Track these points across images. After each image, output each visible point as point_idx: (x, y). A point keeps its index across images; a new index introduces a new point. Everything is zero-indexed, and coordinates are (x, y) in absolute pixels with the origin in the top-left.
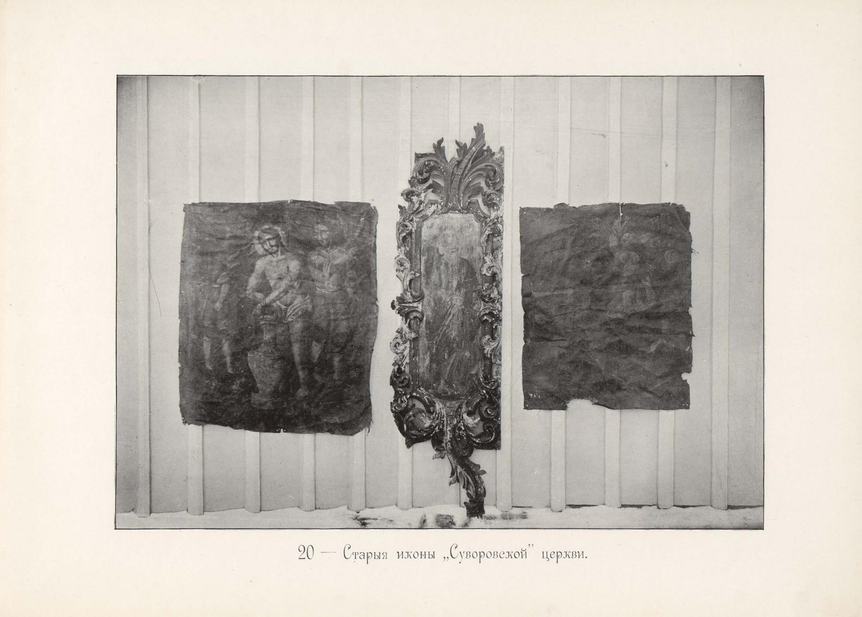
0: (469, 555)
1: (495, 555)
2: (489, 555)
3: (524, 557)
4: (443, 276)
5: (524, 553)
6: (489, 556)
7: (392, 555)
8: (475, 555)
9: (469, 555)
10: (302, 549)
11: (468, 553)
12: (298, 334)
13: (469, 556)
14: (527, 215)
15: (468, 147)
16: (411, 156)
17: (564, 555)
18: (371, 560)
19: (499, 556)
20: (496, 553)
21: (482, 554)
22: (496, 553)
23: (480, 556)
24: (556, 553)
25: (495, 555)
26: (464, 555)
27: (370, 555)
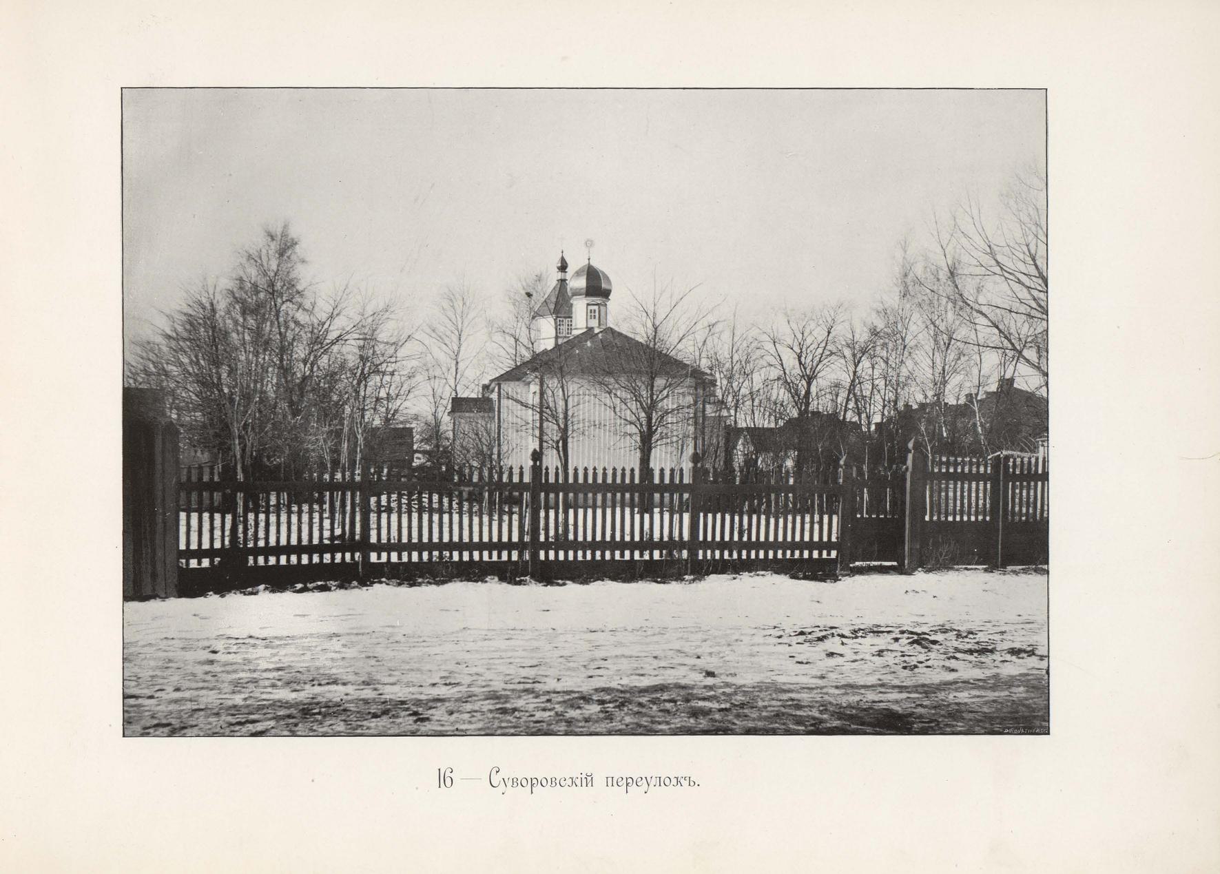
0: (515, 782)
1: (553, 782)
2: (544, 782)
3: (590, 784)
4: (597, 445)
5: (589, 778)
6: (544, 784)
7: (599, 781)
8: (524, 782)
9: (515, 782)
10: (448, 781)
11: (515, 780)
12: (860, 372)
13: (515, 784)
14: (571, 289)
15: (538, 450)
16: (480, 630)
17: (674, 781)
18: (537, 789)
19: (519, 784)
20: (554, 780)
21: (534, 781)
22: (554, 780)
23: (532, 785)
24: (625, 780)
25: (553, 782)
26: (509, 783)
27: (534, 781)
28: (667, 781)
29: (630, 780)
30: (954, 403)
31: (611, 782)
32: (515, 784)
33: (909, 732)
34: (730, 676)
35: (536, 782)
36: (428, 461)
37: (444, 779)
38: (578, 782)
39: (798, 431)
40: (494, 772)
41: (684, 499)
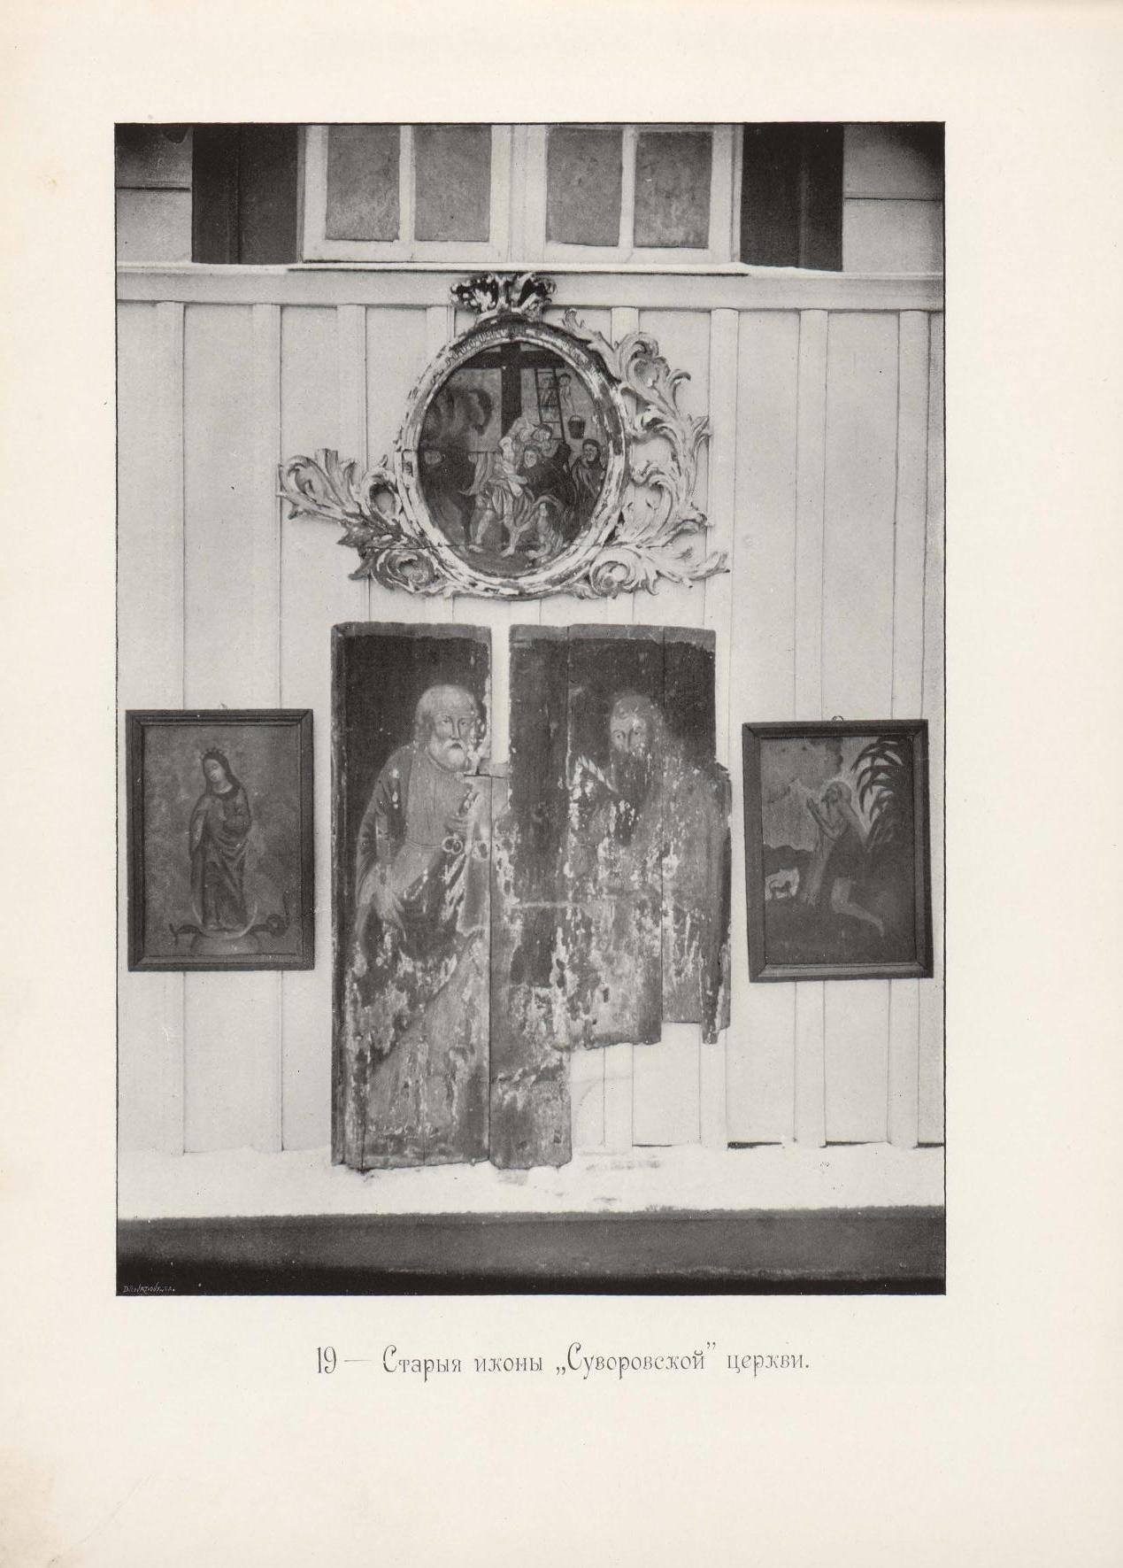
1: (647, 1363)
2: (636, 1363)
3: (699, 1366)
5: (698, 1358)
6: (612, 1362)
8: (612, 1364)
17: (767, 1361)
18: (627, 1372)
19: (606, 1365)
22: (648, 1360)
23: (621, 1366)
25: (647, 1363)
27: (624, 1362)
28: (509, 1364)
29: (759, 1360)
30: (519, 294)
31: (480, 1364)
32: (648, 1365)
33: (334, 1087)
34: (394, 1088)
35: (626, 1363)
36: (433, 959)
37: (326, 1360)
38: (779, 1362)
39: (699, 895)
40: (389, 1352)
41: (396, 793)
